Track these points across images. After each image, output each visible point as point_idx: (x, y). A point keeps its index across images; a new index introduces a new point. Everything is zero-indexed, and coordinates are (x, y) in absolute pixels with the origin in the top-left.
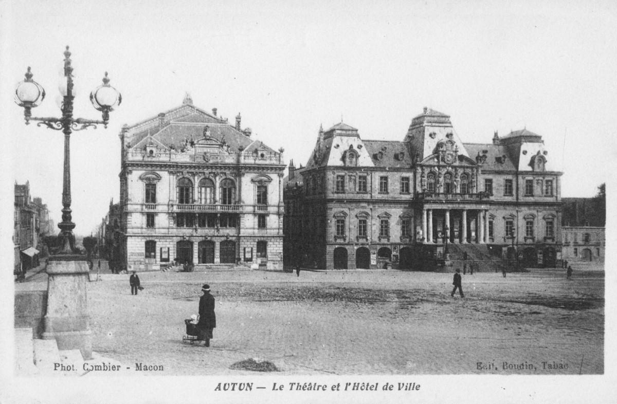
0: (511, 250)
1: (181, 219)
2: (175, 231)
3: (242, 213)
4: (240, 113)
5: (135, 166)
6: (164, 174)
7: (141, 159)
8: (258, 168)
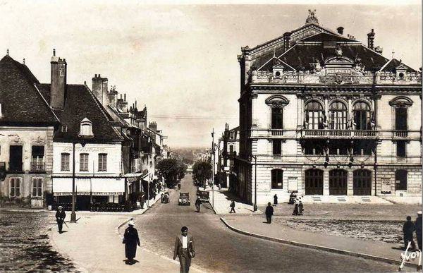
1: (309, 146)
2: (302, 160)
3: (377, 140)
4: (373, 30)
6: (292, 98)
7: (267, 81)
8: (397, 89)
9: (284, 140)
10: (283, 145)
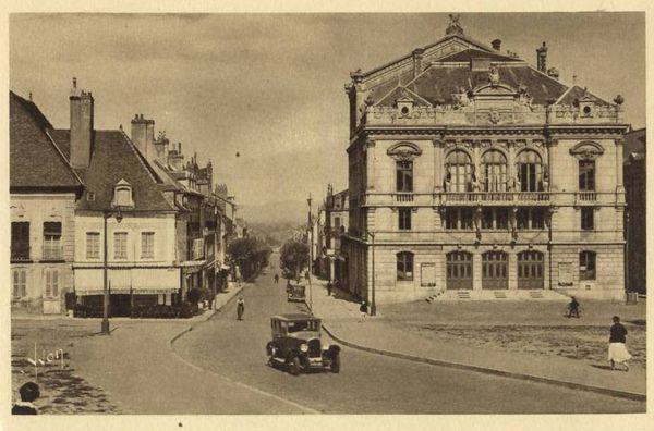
10: (414, 216)
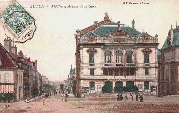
0: (29, 96)
1: (106, 71)
5: (88, 46)
6: (99, 49)
9: (95, 68)
